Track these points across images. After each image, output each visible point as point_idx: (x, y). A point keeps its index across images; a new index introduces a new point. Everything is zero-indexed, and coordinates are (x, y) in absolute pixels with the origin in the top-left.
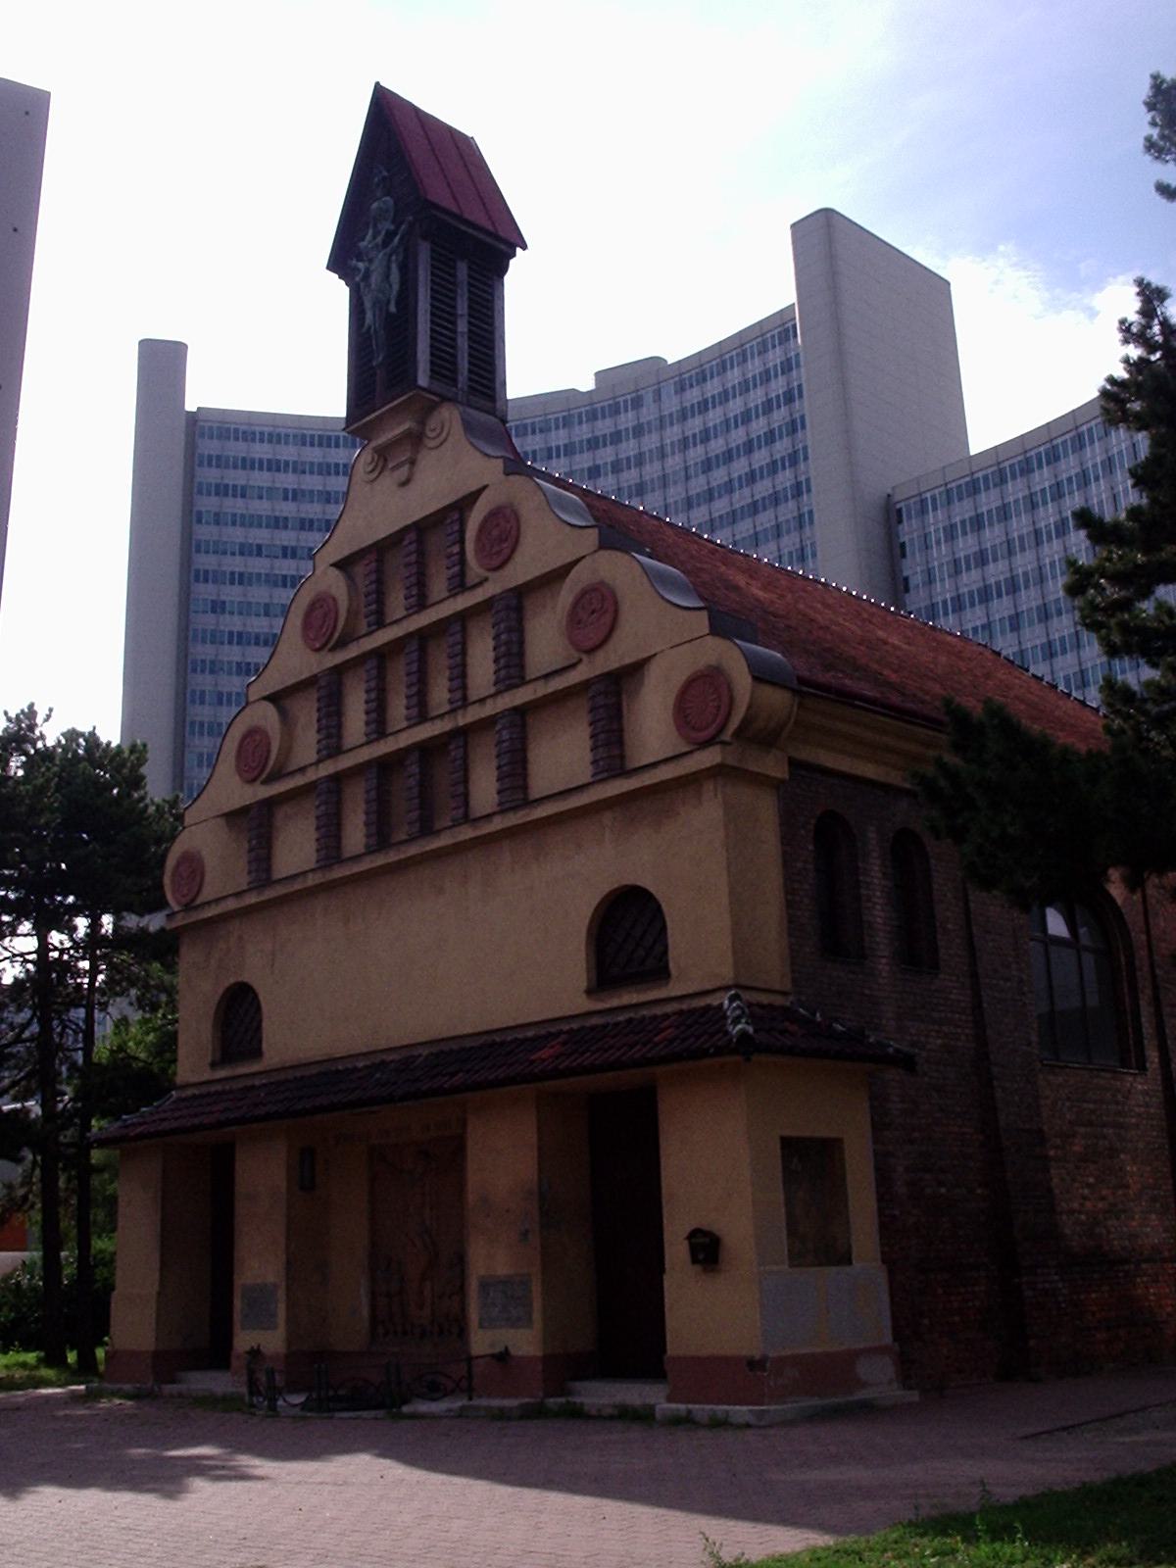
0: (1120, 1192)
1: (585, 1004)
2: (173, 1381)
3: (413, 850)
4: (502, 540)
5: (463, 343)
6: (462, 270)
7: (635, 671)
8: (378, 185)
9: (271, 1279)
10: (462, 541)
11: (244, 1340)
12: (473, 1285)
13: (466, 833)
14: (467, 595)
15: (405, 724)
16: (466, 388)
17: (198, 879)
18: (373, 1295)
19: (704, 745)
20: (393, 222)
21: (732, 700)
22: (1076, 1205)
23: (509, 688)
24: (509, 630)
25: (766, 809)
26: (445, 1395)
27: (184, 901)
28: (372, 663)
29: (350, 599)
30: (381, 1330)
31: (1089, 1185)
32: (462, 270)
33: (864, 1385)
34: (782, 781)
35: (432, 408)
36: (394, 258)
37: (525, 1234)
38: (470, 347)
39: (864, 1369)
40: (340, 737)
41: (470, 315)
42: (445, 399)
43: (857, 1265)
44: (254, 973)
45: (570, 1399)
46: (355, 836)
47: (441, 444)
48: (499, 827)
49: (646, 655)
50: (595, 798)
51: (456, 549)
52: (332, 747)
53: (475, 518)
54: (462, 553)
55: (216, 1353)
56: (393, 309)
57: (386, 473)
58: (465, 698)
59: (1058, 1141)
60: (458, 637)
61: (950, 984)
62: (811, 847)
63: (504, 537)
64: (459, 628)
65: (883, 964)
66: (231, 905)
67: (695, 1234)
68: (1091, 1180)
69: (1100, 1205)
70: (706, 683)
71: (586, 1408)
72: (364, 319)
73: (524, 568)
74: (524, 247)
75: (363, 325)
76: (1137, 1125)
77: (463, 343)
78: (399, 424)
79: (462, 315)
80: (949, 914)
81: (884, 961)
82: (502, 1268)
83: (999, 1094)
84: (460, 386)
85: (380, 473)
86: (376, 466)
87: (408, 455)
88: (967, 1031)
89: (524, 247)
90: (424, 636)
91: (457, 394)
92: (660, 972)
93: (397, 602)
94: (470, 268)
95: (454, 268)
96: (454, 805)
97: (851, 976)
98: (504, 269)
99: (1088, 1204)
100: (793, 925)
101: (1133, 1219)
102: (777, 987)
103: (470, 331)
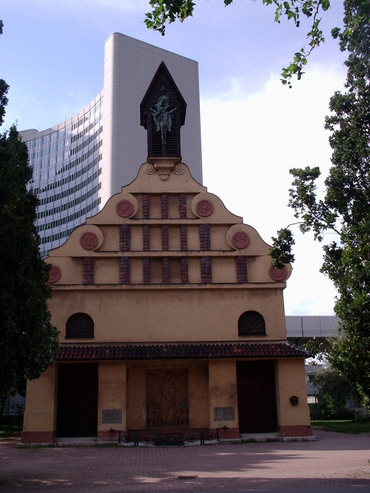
1: (238, 338)
9: (118, 407)
12: (212, 409)
13: (128, 287)
14: (185, 220)
18: (148, 412)
23: (203, 251)
26: (213, 439)
37: (232, 396)
45: (243, 438)
48: (208, 288)
50: (237, 287)
63: (208, 209)
71: (255, 440)
78: (169, 164)
82: (223, 404)
85: (154, 173)
86: (152, 171)
87: (168, 173)
92: (92, 336)
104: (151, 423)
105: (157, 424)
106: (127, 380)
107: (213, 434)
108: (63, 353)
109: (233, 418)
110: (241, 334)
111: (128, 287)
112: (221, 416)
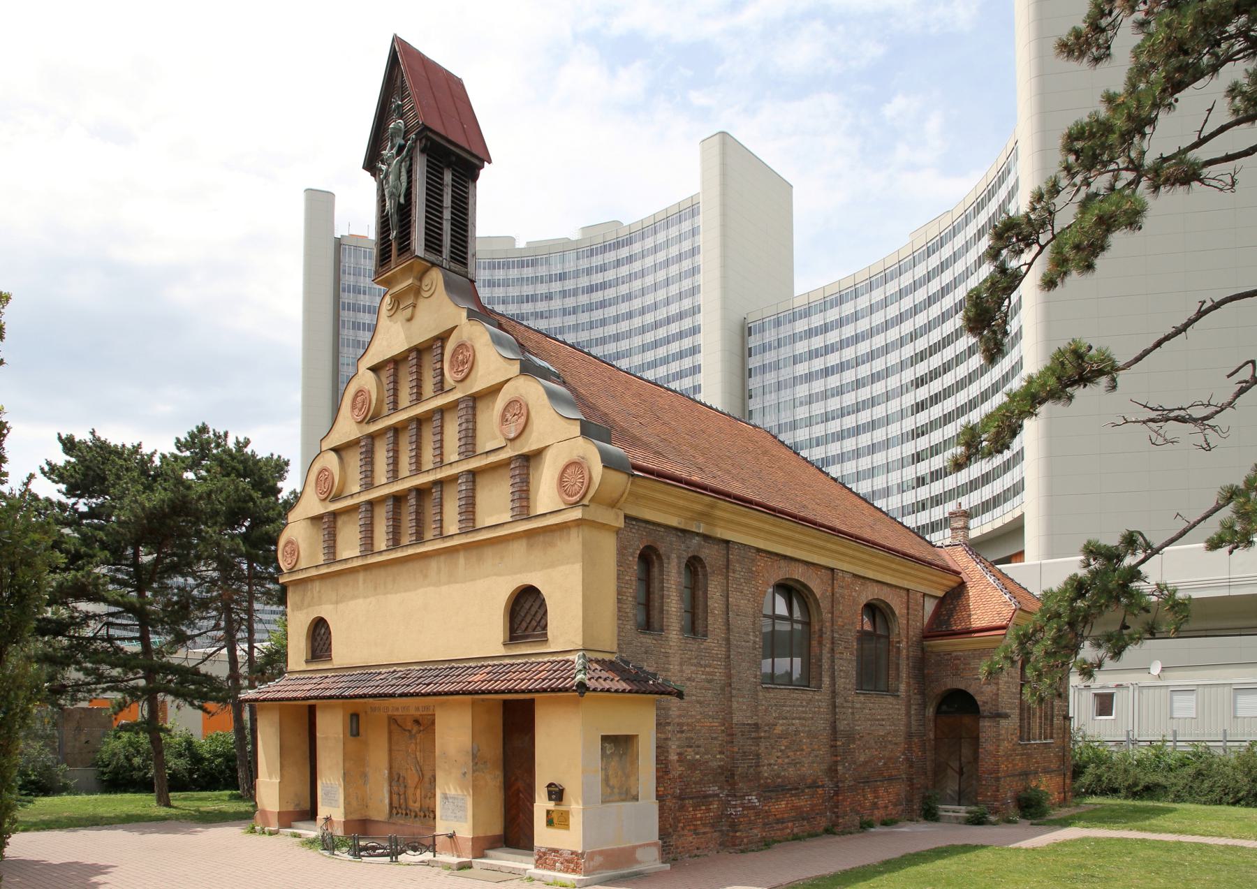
0: (798, 753)
1: (502, 651)
2: (290, 827)
3: (410, 551)
4: (463, 363)
5: (447, 227)
6: (448, 177)
7: (538, 454)
8: (394, 111)
10: (442, 361)
11: (322, 812)
15: (432, 466)
16: (448, 258)
17: (296, 554)
18: (391, 793)
19: (574, 505)
20: (403, 139)
21: (590, 478)
22: (772, 761)
23: (467, 458)
24: (467, 421)
25: (609, 545)
27: (290, 566)
28: (391, 434)
29: (378, 393)
30: (394, 811)
31: (781, 751)
32: (448, 177)
33: (637, 862)
34: (620, 529)
35: (425, 271)
36: (403, 164)
38: (452, 229)
39: (639, 855)
40: (372, 477)
41: (452, 207)
42: (434, 264)
43: (640, 801)
44: (325, 612)
46: (381, 541)
47: (432, 295)
49: (543, 446)
51: (438, 365)
52: (369, 485)
53: (450, 346)
54: (442, 369)
55: (310, 814)
56: (402, 201)
57: (399, 311)
58: (442, 461)
59: (767, 728)
60: (438, 423)
61: (713, 645)
62: (635, 568)
64: (439, 417)
65: (674, 634)
66: (314, 573)
67: (550, 785)
68: (783, 748)
69: (786, 760)
70: (576, 465)
72: (384, 206)
73: (479, 383)
74: (490, 162)
75: (383, 211)
76: (812, 718)
77: (447, 227)
79: (447, 208)
80: (716, 605)
81: (675, 633)
83: (735, 705)
84: (444, 257)
88: (720, 671)
89: (490, 162)
90: (420, 421)
91: (442, 262)
93: (405, 397)
94: (453, 175)
95: (442, 174)
96: (434, 526)
97: (654, 642)
98: (475, 178)
99: (780, 761)
100: (621, 614)
101: (803, 766)
102: (608, 649)
103: (452, 218)
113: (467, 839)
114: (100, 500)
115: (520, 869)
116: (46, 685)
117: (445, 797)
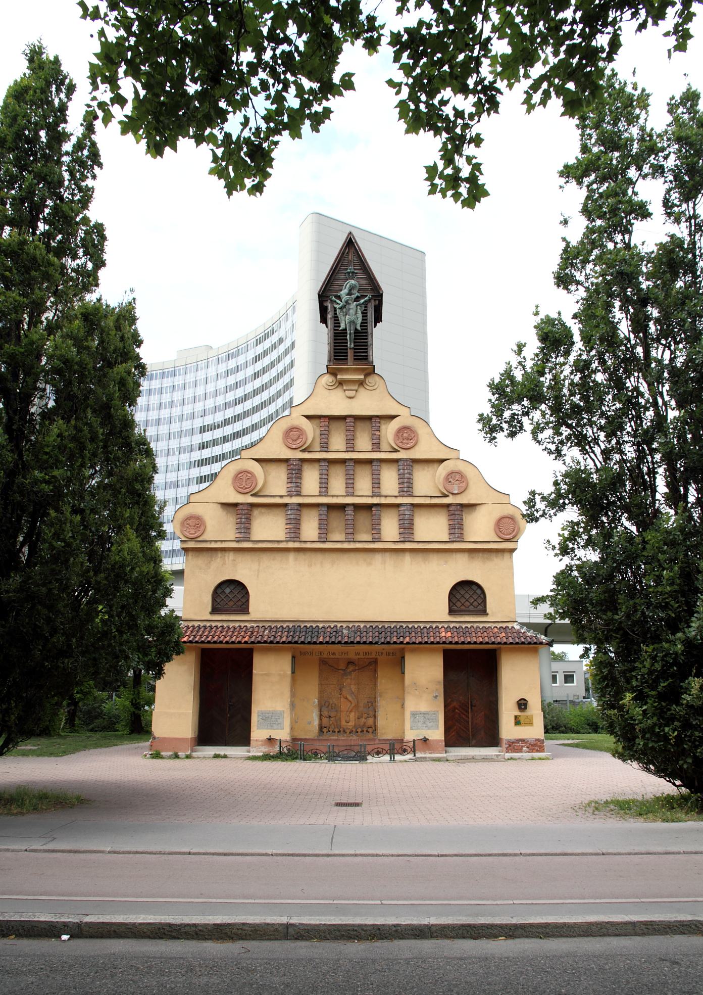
104: (325, 730)
105: (334, 732)
106: (293, 672)
107: (407, 748)
108: (206, 633)
109: (437, 728)
110: (451, 612)
111: (297, 545)
112: (419, 724)
113: (440, 741)
114: (63, 90)
115: (492, 755)
116: (168, 89)
117: (414, 715)
